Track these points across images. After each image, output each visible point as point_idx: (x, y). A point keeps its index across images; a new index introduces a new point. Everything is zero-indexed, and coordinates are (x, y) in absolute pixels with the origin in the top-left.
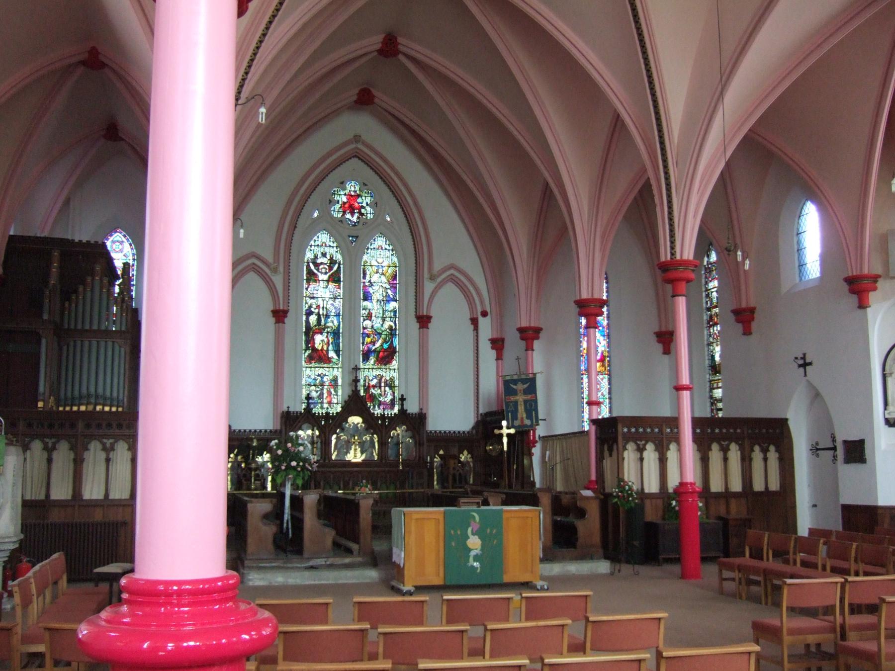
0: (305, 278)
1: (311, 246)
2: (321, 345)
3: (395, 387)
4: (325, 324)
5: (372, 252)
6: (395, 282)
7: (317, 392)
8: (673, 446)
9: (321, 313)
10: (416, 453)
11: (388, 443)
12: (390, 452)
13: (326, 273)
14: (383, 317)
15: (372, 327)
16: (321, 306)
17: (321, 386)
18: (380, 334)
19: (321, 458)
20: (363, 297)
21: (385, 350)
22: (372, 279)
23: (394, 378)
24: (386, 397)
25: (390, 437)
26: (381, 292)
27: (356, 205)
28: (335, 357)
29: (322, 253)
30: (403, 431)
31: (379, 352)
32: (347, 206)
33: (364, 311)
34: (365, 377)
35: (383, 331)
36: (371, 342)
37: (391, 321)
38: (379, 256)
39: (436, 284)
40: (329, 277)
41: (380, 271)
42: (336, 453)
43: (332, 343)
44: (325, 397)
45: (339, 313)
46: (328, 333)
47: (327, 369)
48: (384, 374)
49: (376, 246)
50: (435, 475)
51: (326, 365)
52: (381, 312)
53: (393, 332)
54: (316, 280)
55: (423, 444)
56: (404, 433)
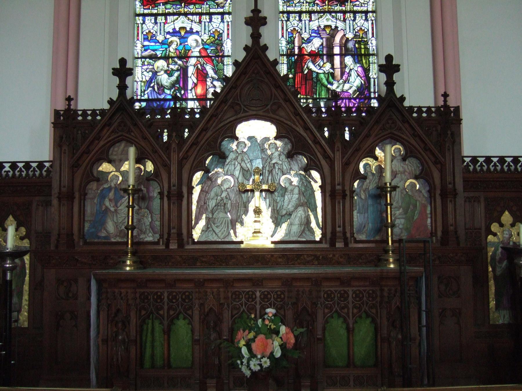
3: (368, 55)
7: (169, 73)
8: (64, 190)
10: (434, 221)
11: (352, 192)
12: (357, 218)
17: (180, 58)
19: (162, 236)
23: (366, 33)
24: (347, 81)
25: (357, 175)
30: (393, 158)
42: (202, 223)
47: (196, 18)
48: (340, 25)
50: (492, 283)
55: (455, 194)
56: (398, 166)
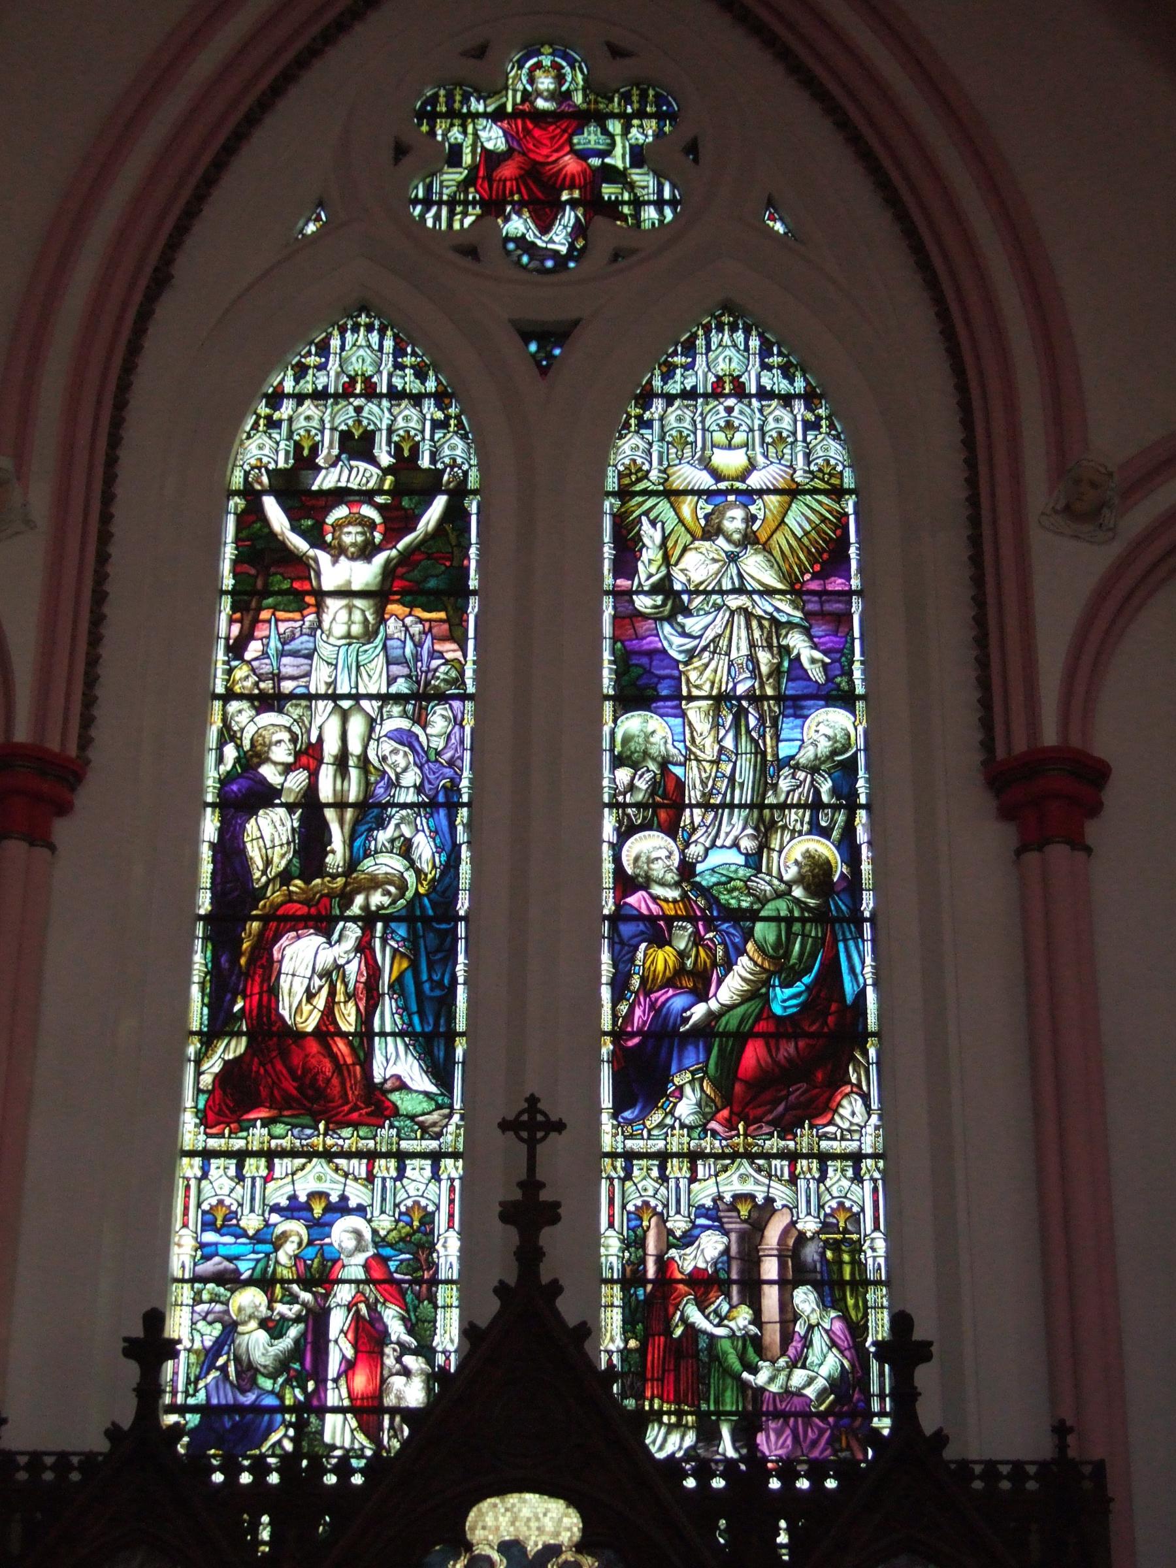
0: (228, 582)
1: (276, 399)
2: (320, 1001)
3: (861, 1283)
4: (352, 865)
5: (677, 417)
6: (836, 584)
7: (274, 1327)
9: (326, 791)
13: (366, 552)
14: (757, 805)
15: (686, 870)
16: (331, 748)
18: (745, 918)
20: (620, 675)
21: (786, 1027)
22: (676, 572)
23: (856, 1218)
24: (799, 1361)
26: (740, 650)
27: (570, 164)
28: (421, 1082)
29: (346, 436)
31: (740, 1038)
32: (508, 170)
33: (623, 775)
34: (638, 1214)
35: (763, 901)
36: (681, 971)
37: (816, 829)
38: (720, 437)
39: (1116, 549)
40: (388, 571)
41: (734, 521)
43: (398, 986)
44: (334, 1366)
45: (453, 788)
46: (368, 919)
47: (359, 1167)
48: (781, 1193)
49: (699, 377)
51: (348, 1139)
52: (746, 771)
53: (840, 905)
54: (299, 595)
